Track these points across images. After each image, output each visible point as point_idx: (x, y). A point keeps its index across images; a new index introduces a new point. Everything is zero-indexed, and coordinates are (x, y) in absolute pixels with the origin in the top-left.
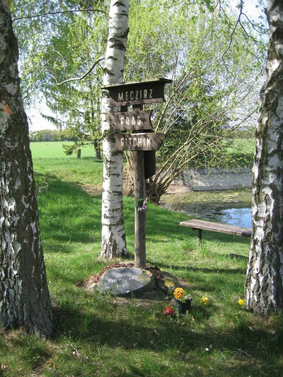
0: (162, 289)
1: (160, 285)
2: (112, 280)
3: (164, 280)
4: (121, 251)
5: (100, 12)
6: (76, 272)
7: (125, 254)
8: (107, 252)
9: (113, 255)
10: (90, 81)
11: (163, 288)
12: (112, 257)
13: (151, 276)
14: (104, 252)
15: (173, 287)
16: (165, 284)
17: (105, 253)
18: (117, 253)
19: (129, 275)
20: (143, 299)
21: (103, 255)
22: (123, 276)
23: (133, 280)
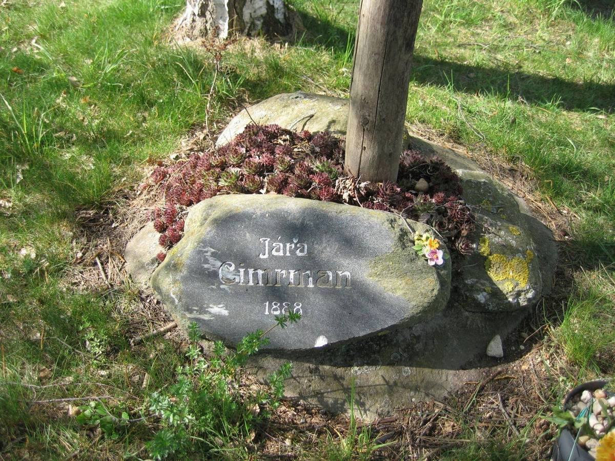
0: (478, 304)
1: (469, 281)
2: (237, 271)
3: (484, 249)
4: (264, 11)
5: (129, 226)
6: (61, 155)
7: (277, 21)
8: (208, 14)
9: (231, 25)
10: (174, 132)
11: (481, 297)
12: (230, 34)
13: (440, 262)
14: (197, 10)
15: (527, 291)
16: (492, 274)
17: (202, 14)
18: (246, 17)
19: (327, 250)
20: (391, 364)
21: (194, 21)
22: (293, 252)
23: (345, 279)
